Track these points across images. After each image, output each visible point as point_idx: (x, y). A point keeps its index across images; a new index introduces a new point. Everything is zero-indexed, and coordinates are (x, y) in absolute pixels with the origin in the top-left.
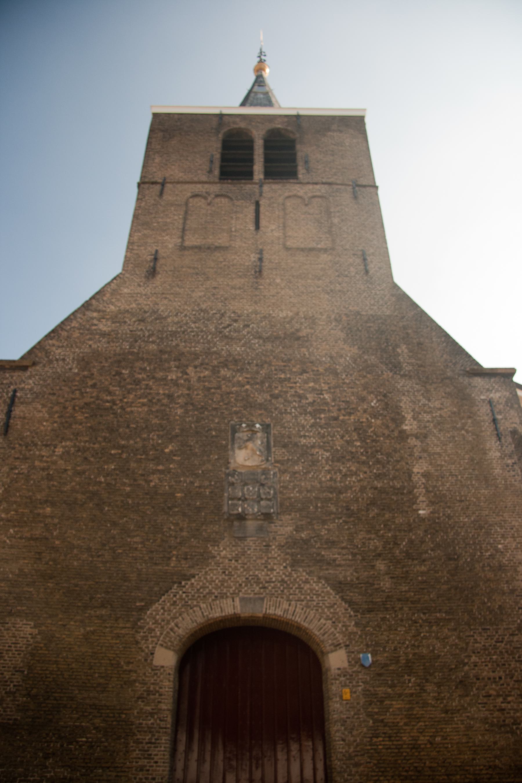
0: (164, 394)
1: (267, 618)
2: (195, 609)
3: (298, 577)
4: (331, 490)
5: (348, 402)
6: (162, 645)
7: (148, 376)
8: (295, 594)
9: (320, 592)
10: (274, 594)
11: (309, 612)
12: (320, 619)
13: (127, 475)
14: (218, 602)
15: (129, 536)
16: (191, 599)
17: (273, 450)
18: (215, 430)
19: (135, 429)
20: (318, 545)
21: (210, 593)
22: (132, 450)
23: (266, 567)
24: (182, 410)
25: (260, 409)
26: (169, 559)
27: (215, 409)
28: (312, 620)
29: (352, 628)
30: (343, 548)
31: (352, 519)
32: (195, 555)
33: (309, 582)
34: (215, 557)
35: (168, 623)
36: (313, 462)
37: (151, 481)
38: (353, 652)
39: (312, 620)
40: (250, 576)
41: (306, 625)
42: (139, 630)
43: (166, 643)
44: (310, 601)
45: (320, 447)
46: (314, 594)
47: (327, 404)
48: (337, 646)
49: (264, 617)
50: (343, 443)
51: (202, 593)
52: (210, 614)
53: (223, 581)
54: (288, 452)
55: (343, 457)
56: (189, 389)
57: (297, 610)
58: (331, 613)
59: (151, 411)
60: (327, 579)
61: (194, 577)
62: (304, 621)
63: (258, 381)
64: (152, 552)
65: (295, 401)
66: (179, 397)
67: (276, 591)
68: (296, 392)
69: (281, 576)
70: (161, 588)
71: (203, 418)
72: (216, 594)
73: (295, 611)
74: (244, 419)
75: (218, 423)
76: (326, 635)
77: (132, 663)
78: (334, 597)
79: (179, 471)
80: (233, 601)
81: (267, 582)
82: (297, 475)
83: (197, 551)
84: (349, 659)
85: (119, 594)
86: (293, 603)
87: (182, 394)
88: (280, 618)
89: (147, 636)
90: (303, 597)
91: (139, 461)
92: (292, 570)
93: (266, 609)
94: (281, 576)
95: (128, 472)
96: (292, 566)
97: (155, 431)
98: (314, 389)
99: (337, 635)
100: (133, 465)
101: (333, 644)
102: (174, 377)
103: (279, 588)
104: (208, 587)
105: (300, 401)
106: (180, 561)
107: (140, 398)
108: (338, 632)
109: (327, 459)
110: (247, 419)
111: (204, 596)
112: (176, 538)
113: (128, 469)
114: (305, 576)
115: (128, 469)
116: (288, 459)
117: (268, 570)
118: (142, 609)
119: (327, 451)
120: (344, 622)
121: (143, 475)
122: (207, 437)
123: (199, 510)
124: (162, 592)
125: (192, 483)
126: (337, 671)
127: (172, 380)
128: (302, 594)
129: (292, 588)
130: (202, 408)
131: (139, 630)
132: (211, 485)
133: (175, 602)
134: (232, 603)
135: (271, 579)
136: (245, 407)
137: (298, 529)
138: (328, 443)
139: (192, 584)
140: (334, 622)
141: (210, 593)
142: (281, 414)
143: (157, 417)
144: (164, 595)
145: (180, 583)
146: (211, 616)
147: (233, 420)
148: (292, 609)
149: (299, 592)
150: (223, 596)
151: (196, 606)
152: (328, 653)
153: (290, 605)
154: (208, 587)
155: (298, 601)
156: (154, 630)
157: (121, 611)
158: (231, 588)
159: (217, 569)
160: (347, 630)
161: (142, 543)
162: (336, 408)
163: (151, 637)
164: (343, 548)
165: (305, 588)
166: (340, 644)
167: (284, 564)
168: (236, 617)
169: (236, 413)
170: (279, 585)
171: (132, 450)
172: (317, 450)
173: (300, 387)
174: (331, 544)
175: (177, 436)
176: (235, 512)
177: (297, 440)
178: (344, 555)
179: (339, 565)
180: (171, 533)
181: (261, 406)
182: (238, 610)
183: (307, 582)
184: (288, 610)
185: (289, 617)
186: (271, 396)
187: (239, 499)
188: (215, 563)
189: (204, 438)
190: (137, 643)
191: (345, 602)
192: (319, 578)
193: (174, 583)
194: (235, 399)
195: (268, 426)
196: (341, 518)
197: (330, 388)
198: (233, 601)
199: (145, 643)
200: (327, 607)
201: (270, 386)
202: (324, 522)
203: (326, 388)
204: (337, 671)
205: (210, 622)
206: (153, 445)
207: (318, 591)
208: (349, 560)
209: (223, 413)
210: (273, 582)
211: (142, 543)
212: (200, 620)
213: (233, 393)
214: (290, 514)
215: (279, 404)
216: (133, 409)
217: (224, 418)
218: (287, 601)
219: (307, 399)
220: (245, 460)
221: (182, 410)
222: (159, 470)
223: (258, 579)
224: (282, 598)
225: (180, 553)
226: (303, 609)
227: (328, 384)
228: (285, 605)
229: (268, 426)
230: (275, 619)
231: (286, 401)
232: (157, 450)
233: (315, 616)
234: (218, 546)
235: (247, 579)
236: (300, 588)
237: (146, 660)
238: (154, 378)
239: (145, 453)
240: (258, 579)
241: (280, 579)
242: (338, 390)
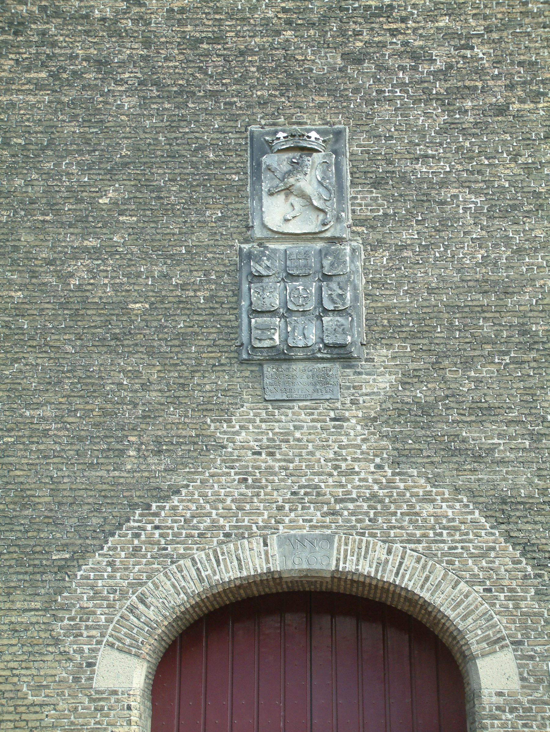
0: (87, 59)
1: (339, 579)
2: (181, 562)
3: (406, 489)
4: (485, 286)
5: (532, 64)
6: (112, 645)
7: (43, 9)
8: (401, 528)
9: (457, 523)
10: (353, 527)
11: (433, 567)
12: (457, 584)
13: (14, 262)
14: (231, 545)
15: (28, 406)
16: (172, 542)
17: (350, 192)
18: (214, 147)
19: (24, 148)
20: (454, 416)
21: (215, 527)
22: (22, 202)
23: (336, 467)
24: (134, 100)
25: (319, 92)
26: (122, 453)
27: (213, 95)
28: (439, 584)
29: (529, 603)
30: (509, 423)
31: (533, 354)
32: (179, 444)
33: (433, 501)
34: (224, 447)
35: (124, 595)
36: (443, 221)
37: (71, 275)
38: (532, 658)
39: (439, 584)
40: (300, 487)
41: (426, 595)
42: (60, 614)
43: (119, 640)
44: (436, 541)
45: (462, 184)
46: (444, 528)
47: (480, 72)
48: (496, 643)
49: (333, 577)
50: (517, 171)
51: (196, 528)
52: (215, 573)
53: (240, 502)
54: (384, 197)
55: (514, 207)
56: (147, 43)
57: (406, 562)
58: (481, 569)
59: (59, 102)
60: (473, 494)
61: (177, 492)
62: (422, 587)
63: (315, 18)
64: (81, 439)
65: (402, 68)
66: (123, 64)
67: (359, 521)
68: (405, 44)
69: (368, 488)
70: (105, 519)
71: (183, 118)
72: (227, 529)
73: (401, 564)
74: (282, 120)
75: (219, 131)
76: (470, 620)
77: (47, 687)
78: (489, 535)
79: (135, 249)
80: (266, 544)
81: (337, 501)
82: (406, 253)
83: (184, 433)
84: (521, 674)
85: (12, 536)
86: (397, 547)
87: (130, 56)
88: (368, 581)
89: (77, 627)
90: (418, 533)
91: (39, 229)
92: (393, 474)
93: (338, 560)
94: (368, 488)
95: (15, 256)
96: (395, 463)
97: (69, 153)
98: (449, 35)
99: (496, 618)
100: (26, 238)
101: (486, 639)
102: (108, 13)
103: (367, 514)
104: (209, 515)
105: (414, 69)
106: (145, 458)
107: (28, 69)
108: (498, 613)
109: (477, 214)
110: (288, 118)
111: (200, 535)
112: (135, 405)
113: (16, 249)
114: (422, 486)
115: (16, 249)
116: (386, 215)
117: (340, 474)
118: (63, 568)
119: (476, 192)
120: (511, 590)
121: (51, 262)
122: (194, 165)
123: (183, 339)
124: (107, 528)
125: (165, 276)
126: (494, 699)
127: (104, 19)
128: (417, 528)
129: (395, 514)
130: (179, 93)
131: (60, 614)
132: (209, 281)
133: (137, 549)
134: (262, 548)
135: (349, 493)
136: (283, 88)
137: (408, 379)
138: (479, 172)
139: (174, 508)
140: (489, 590)
141: (215, 527)
142: (369, 102)
143: (74, 117)
144: (113, 534)
145: (149, 507)
146: (217, 577)
147: (255, 122)
148: (394, 560)
149: (410, 521)
150: (241, 533)
151: (183, 556)
152: (478, 657)
153: (389, 552)
154: (209, 515)
155: (409, 542)
156: (94, 613)
157: (18, 573)
158: (262, 514)
159: (228, 474)
160: (517, 607)
161: (59, 419)
162: (502, 82)
163: (87, 628)
164: (509, 423)
165: (425, 514)
166: (503, 639)
167: (378, 460)
168: (273, 578)
169: (263, 103)
170: (365, 505)
171: (22, 202)
172: (454, 191)
173: (415, 30)
174: (483, 412)
175: (125, 165)
176: (267, 344)
177: (406, 166)
178: (511, 438)
179: (502, 462)
180: (123, 393)
181: (324, 85)
182: (277, 565)
183: (428, 499)
184: (387, 561)
185: (389, 577)
186: (344, 56)
187: (273, 313)
188: (223, 461)
189: (190, 170)
190: (57, 641)
191: (514, 545)
192: (457, 490)
193: (133, 506)
194: (259, 69)
195: (338, 134)
196: (507, 353)
197: (488, 30)
198: (266, 544)
199: (75, 643)
200: (472, 556)
201: (342, 32)
202: (467, 363)
203: (481, 30)
204: (494, 699)
205: (215, 591)
206: (69, 189)
207: (453, 520)
208: (524, 449)
209: (232, 104)
210: (353, 500)
211: (59, 419)
212: (195, 587)
213: (254, 54)
214: (389, 346)
215: (364, 76)
216: (14, 98)
217: (234, 118)
218: (384, 542)
219: (432, 61)
220: (286, 220)
221: (134, 100)
222: (87, 250)
223: (318, 494)
224: (373, 535)
225: (145, 439)
226: (418, 561)
227: (485, 18)
228: (380, 552)
229: (338, 134)
230: (358, 582)
231: (380, 68)
232: (81, 201)
233: (446, 575)
234: (229, 421)
235: (294, 493)
236: (412, 513)
237: (76, 680)
238: (57, 14)
239: (52, 207)
240: (318, 494)
241: (367, 493)
242: (507, 35)
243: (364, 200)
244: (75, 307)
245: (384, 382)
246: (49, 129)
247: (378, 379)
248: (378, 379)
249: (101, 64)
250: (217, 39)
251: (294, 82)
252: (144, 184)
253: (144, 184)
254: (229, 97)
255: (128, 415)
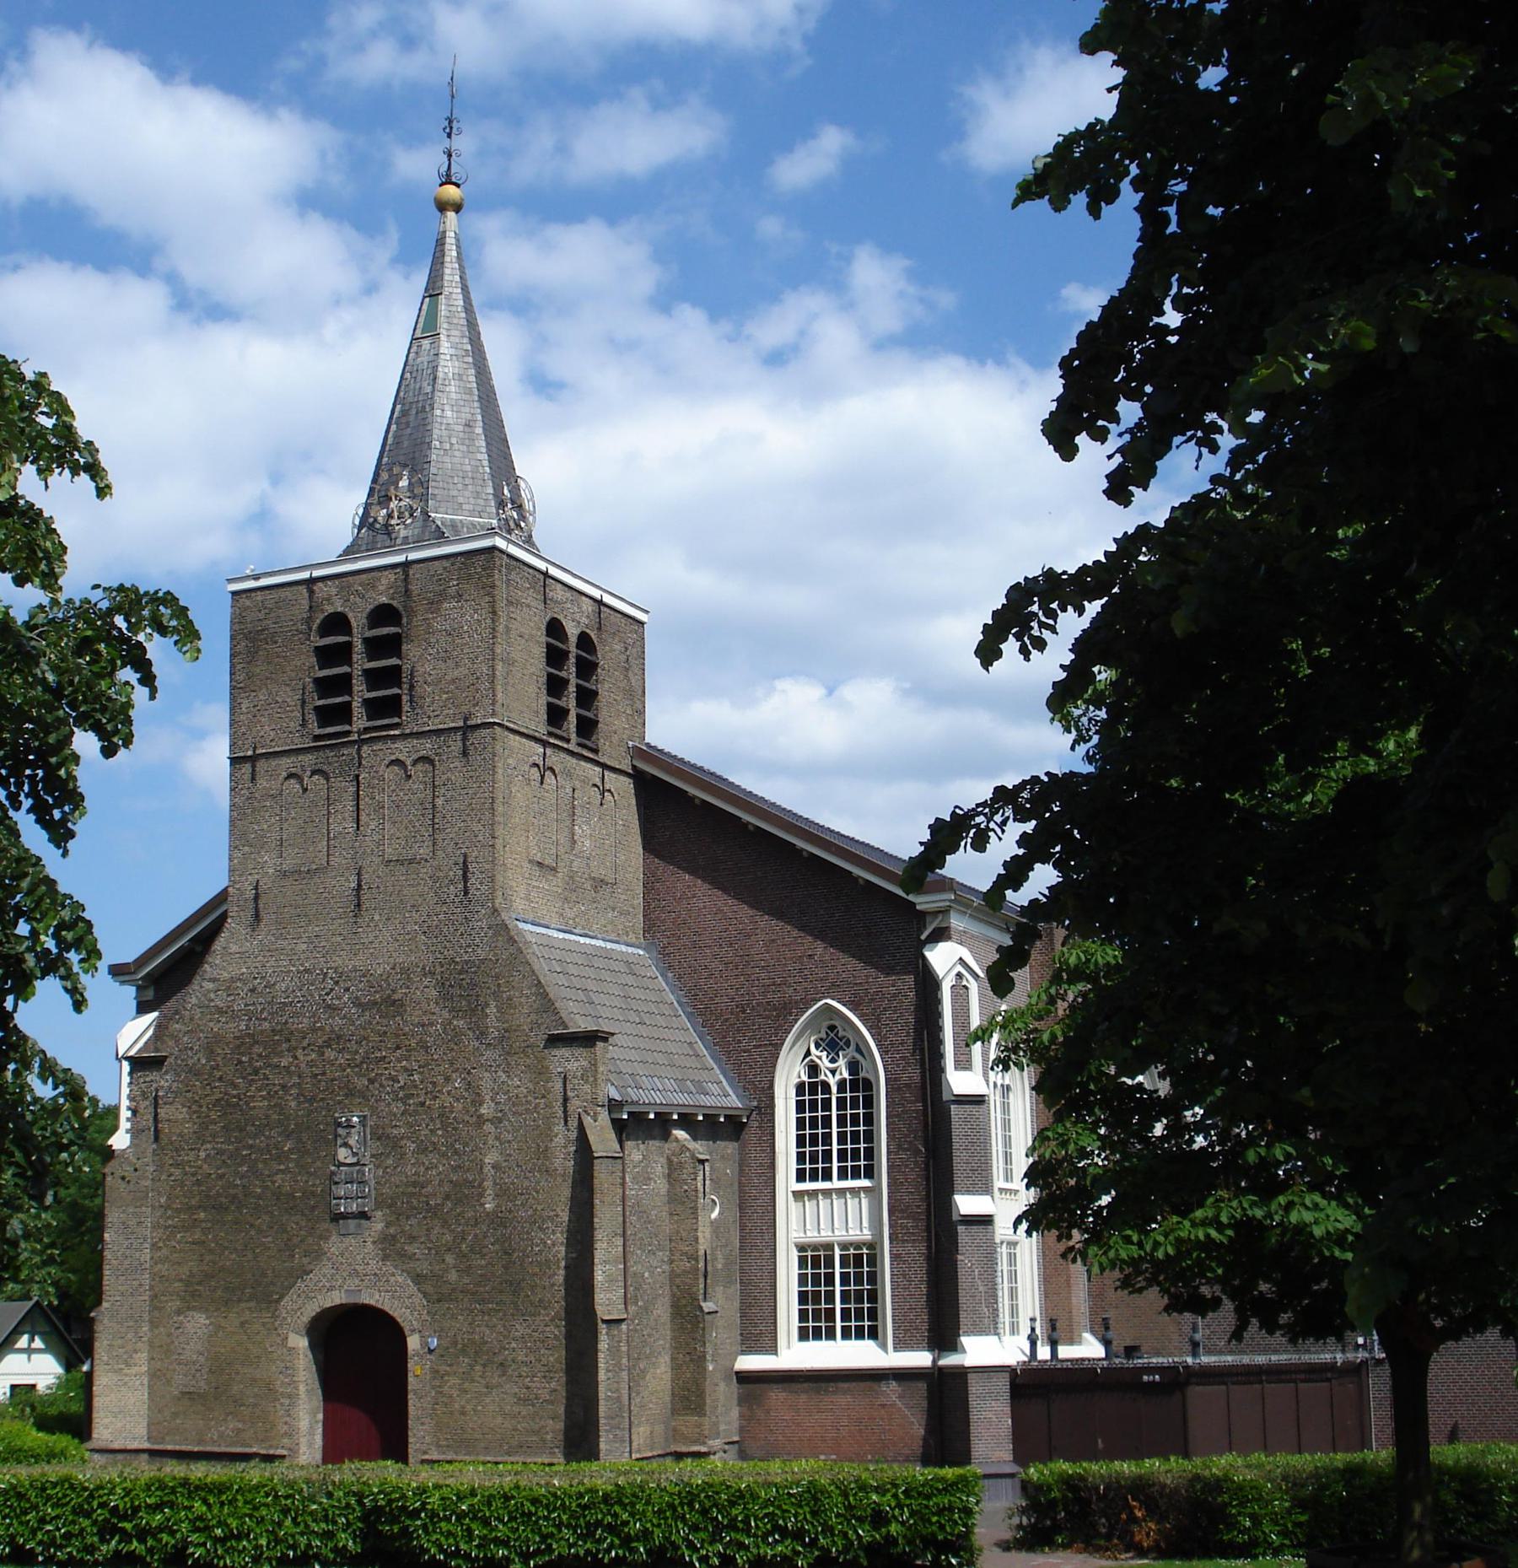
4: (415, 1185)
47: (416, 1087)
78: (413, 1289)
91: (265, 1161)
98: (406, 1069)
118: (278, 1301)
123: (313, 1208)
150: (331, 1289)
169: (340, 1103)
174: (412, 1239)
177: (389, 1130)
202: (408, 1218)
243: (374, 1146)
244: (278, 1195)
245: (380, 1226)
246: (267, 1117)
247: (378, 1226)
248: (378, 1226)
249: (283, 1087)
250: (324, 1074)
251: (350, 1093)
252: (300, 1140)
253: (300, 1140)
254: (548, 1106)
255: (296, 1240)
